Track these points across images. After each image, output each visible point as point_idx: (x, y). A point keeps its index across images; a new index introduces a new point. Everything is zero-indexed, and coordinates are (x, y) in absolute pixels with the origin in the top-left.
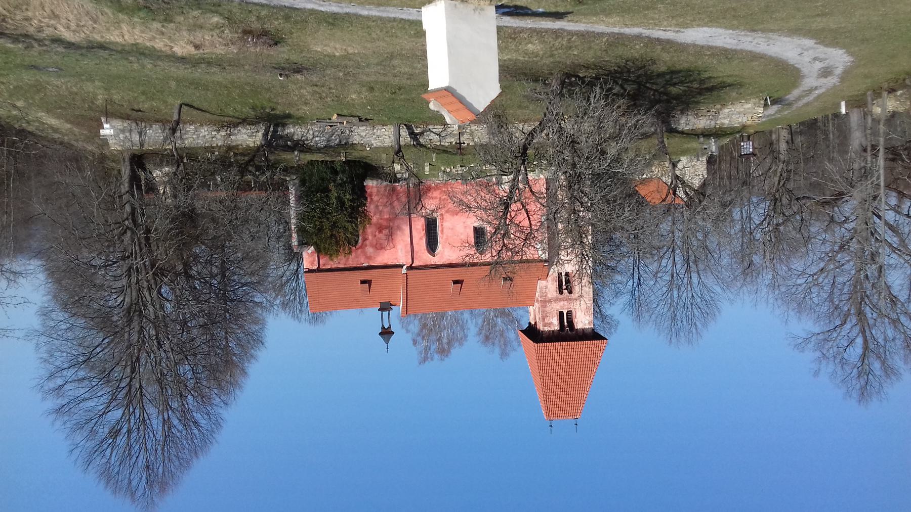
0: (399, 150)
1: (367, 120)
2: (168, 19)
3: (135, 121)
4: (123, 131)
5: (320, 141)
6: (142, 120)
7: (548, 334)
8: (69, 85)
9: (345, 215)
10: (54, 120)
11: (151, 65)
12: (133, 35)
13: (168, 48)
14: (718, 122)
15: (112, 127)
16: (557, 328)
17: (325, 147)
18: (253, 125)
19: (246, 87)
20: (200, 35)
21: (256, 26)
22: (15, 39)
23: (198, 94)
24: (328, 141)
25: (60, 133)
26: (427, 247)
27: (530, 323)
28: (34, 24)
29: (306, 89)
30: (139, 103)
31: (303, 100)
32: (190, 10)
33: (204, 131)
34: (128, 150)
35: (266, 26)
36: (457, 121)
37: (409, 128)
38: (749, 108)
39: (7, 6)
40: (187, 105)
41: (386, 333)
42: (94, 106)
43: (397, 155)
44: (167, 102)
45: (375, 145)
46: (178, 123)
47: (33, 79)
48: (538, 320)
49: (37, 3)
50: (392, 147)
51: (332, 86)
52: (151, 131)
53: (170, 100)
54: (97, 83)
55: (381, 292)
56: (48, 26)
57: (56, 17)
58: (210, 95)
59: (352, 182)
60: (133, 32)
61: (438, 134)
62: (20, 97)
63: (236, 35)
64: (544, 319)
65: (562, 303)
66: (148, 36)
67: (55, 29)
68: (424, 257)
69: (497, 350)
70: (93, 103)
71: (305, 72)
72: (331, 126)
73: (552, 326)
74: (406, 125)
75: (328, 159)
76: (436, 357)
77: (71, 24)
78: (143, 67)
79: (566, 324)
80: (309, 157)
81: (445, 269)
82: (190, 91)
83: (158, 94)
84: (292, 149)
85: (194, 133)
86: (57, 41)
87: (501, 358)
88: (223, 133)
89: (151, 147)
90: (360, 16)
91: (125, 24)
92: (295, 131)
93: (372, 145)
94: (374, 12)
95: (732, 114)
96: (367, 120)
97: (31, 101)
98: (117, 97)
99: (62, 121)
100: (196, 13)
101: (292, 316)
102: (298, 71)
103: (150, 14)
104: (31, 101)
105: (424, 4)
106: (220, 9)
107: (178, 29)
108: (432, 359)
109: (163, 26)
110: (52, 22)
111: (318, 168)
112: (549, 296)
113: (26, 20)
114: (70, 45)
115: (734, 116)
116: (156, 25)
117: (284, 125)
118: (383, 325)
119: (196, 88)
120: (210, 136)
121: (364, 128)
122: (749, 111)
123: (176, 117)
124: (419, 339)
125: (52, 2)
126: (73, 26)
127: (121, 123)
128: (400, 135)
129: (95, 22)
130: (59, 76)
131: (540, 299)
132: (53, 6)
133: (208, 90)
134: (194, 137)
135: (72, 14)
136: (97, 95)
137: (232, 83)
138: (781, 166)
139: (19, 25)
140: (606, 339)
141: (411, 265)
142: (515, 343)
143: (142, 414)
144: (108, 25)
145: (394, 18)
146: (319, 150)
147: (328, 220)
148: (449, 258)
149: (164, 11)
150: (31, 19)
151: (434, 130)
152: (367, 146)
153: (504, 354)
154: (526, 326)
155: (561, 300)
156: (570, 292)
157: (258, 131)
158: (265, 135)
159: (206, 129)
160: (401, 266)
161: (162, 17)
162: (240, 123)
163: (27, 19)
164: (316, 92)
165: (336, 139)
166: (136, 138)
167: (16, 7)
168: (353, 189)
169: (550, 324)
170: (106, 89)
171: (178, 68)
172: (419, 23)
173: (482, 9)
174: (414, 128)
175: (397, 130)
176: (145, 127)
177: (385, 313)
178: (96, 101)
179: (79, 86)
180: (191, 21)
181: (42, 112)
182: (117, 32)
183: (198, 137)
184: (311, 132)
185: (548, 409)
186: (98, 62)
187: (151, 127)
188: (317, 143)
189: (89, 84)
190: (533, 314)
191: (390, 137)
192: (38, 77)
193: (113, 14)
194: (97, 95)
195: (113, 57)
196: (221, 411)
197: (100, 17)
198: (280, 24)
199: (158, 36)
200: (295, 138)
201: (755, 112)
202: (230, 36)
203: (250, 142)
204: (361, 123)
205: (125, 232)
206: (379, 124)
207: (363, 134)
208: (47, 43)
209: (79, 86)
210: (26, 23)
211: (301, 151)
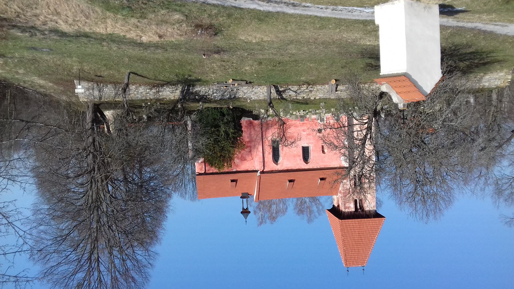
0: (271, 103)
1: (250, 82)
2: (143, 16)
3: (97, 82)
4: (88, 89)
5: (217, 96)
6: (101, 82)
7: (347, 213)
8: (55, 60)
9: (229, 142)
10: (42, 81)
11: (116, 48)
12: (114, 27)
13: (138, 37)
14: (481, 85)
15: (83, 87)
16: (353, 210)
17: (220, 99)
18: (174, 85)
19: (176, 62)
20: (165, 28)
21: (206, 21)
22: (23, 30)
23: (142, 66)
24: (222, 96)
25: (45, 88)
26: (273, 159)
27: (334, 206)
28: (41, 19)
29: (216, 63)
30: (101, 71)
31: (213, 70)
32: (161, 10)
33: (141, 89)
34: (91, 101)
35: (213, 22)
36: (402, 100)
37: (276, 87)
38: (502, 76)
39: (21, 5)
40: (132, 73)
41: (245, 212)
42: (71, 74)
43: (269, 105)
44: (120, 71)
45: (253, 98)
46: (127, 85)
47: (31, 56)
48: (340, 205)
49: (44, 3)
50: (264, 100)
51: (235, 61)
52: (107, 89)
53: (123, 70)
54: (74, 59)
55: (243, 186)
56: (51, 21)
57: (58, 14)
58: (150, 67)
59: (234, 121)
60: (115, 26)
61: (295, 92)
62: (22, 67)
63: (190, 28)
64: (345, 205)
66: (126, 28)
67: (57, 23)
68: (271, 166)
69: (306, 218)
70: (70, 71)
71: (222, 53)
72: (226, 87)
73: (350, 209)
74: (274, 86)
75: (219, 106)
76: (268, 221)
77: (69, 19)
78: (110, 49)
79: (358, 207)
80: (207, 105)
81: (284, 173)
82: (137, 65)
83: (115, 66)
84: (198, 101)
85: (135, 90)
86: (55, 31)
87: (308, 223)
88: (154, 91)
89: (107, 99)
90: (287, 14)
91: (110, 20)
92: (200, 89)
93: (251, 98)
94: (327, 12)
95: (491, 80)
96: (250, 82)
97: (28, 70)
98: (86, 68)
99: (47, 81)
100: (163, 12)
101: (180, 196)
102: (218, 52)
103: (130, 12)
104: (28, 70)
105: (378, 3)
106: (183, 9)
107: (150, 24)
108: (265, 222)
109: (139, 21)
110: (55, 18)
111: (212, 112)
113: (35, 16)
114: (63, 34)
115: (492, 81)
116: (134, 20)
117: (194, 86)
118: (243, 207)
119: (141, 63)
120: (145, 92)
121: (247, 87)
122: (502, 77)
123: (126, 81)
124: (258, 211)
125: (56, 3)
126: (70, 21)
127: (87, 84)
128: (271, 92)
129: (87, 18)
130: (49, 54)
131: (342, 191)
132: (56, 6)
133: (149, 63)
134: (135, 93)
135: (71, 12)
136: (73, 66)
137: (168, 59)
138: (493, 109)
139: (29, 20)
140: (385, 217)
141: (263, 170)
142: (317, 214)
143: (99, 277)
144: (96, 20)
145: (311, 15)
146: (216, 101)
147: (218, 146)
148: (286, 166)
149: (141, 10)
150: (39, 15)
151: (292, 89)
152: (248, 99)
153: (310, 220)
154: (330, 207)
157: (177, 89)
158: (182, 92)
159: (143, 88)
160: (257, 171)
161: (139, 15)
162: (165, 84)
163: (36, 16)
164: (222, 65)
165: (227, 95)
166: (96, 93)
167: (28, 6)
168: (235, 126)
169: (349, 208)
170: (79, 62)
171: (134, 50)
172: (372, 22)
173: (430, 8)
174: (280, 88)
175: (269, 89)
176: (103, 86)
177: (245, 200)
178: (73, 70)
179: (62, 60)
180: (159, 17)
181: (36, 76)
182: (103, 26)
183: (138, 93)
184: (211, 90)
185: (346, 260)
186: (79, 45)
187: (107, 86)
188: (215, 97)
189: (68, 59)
190: (337, 200)
191: (263, 93)
192: (35, 55)
193: (102, 12)
194: (73, 66)
195: (92, 42)
196: (149, 270)
197: (92, 14)
198: (223, 20)
199: (134, 29)
200: (201, 94)
201: (506, 78)
202: (186, 28)
203: (172, 97)
204: (247, 85)
205: (89, 154)
206: (257, 85)
207: (245, 91)
208: (46, 33)
209: (62, 60)
210: (34, 18)
211: (204, 102)
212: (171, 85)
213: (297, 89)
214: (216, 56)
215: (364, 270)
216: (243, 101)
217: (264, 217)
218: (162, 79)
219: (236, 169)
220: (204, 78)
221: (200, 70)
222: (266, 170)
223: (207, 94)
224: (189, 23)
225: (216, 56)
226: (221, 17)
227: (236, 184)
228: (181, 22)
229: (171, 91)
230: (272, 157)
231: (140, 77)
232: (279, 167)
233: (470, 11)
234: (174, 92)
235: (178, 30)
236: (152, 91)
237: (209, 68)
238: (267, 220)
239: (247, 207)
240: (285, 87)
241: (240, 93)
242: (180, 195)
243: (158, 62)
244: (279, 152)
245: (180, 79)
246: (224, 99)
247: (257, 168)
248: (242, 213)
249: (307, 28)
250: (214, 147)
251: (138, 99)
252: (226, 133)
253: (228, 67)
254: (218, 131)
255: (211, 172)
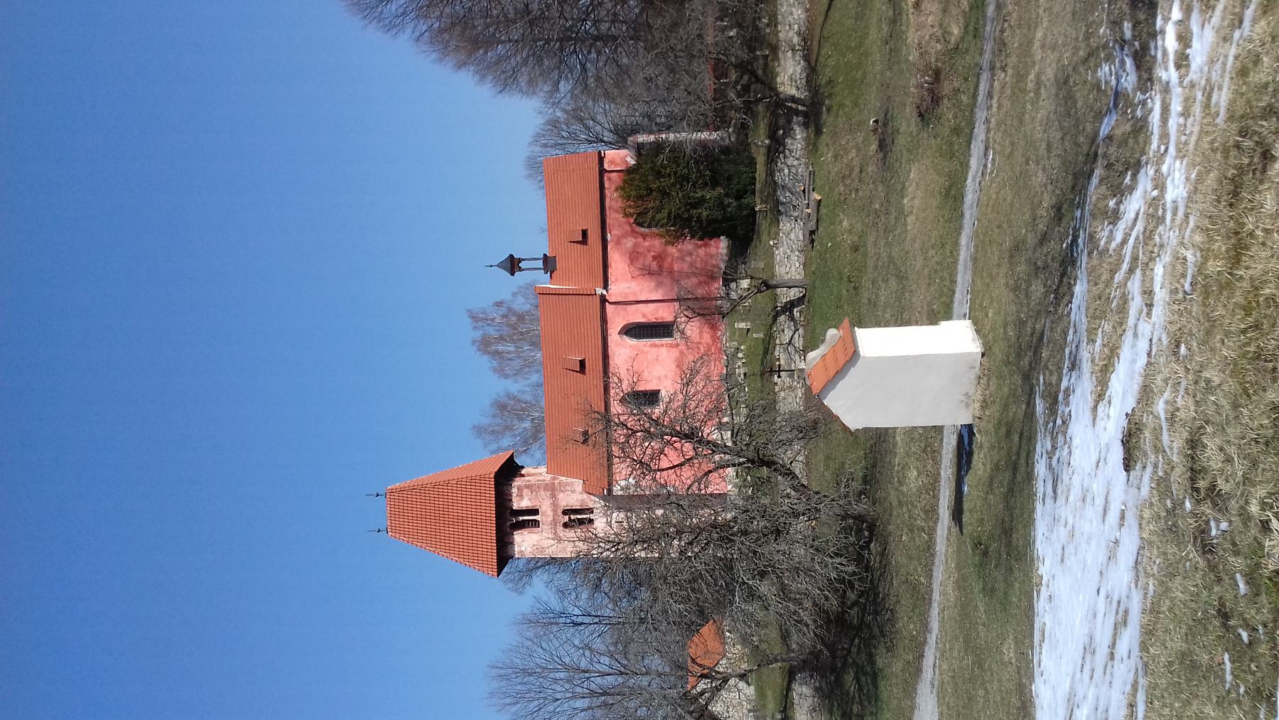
0: (769, 287)
1: (812, 241)
5: (783, 176)
9: (679, 209)
16: (515, 506)
17: (775, 183)
18: (807, 82)
19: (860, 72)
20: (933, 9)
21: (946, 88)
23: (850, 6)
24: (783, 187)
27: (523, 467)
31: (842, 153)
35: (946, 101)
36: (811, 366)
37: (800, 301)
41: (512, 265)
48: (527, 478)
50: (773, 276)
51: (860, 193)
59: (725, 219)
61: (790, 341)
63: (933, 60)
64: (528, 487)
65: (550, 513)
68: (618, 320)
69: (485, 421)
71: (881, 155)
72: (804, 191)
74: (804, 296)
75: (758, 186)
76: (478, 334)
79: (521, 518)
80: (761, 160)
84: (772, 136)
87: (474, 427)
90: (959, 234)
92: (797, 140)
93: (777, 248)
96: (812, 241)
102: (882, 146)
105: (975, 323)
108: (475, 328)
112: (561, 496)
117: (806, 125)
118: (523, 260)
124: (503, 310)
128: (790, 288)
140: (498, 576)
142: (494, 446)
146: (770, 173)
148: (617, 354)
151: (796, 336)
152: (776, 242)
153: (480, 430)
154: (518, 461)
155: (555, 511)
156: (565, 525)
157: (798, 89)
158: (793, 99)
159: (801, 16)
160: (606, 287)
162: (809, 63)
164: (852, 171)
165: (785, 197)
168: (716, 220)
169: (521, 496)
172: (948, 316)
173: (967, 405)
174: (799, 308)
177: (540, 264)
184: (796, 163)
185: (402, 490)
188: (781, 170)
190: (535, 472)
191: (787, 273)
196: (408, 31)
200: (788, 141)
204: (807, 234)
207: (792, 236)
211: (769, 148)
212: (808, 76)
213: (797, 345)
214: (874, 146)
215: (379, 531)
216: (772, 232)
217: (488, 325)
218: (823, 52)
219: (612, 240)
220: (825, 138)
221: (841, 126)
222: (609, 308)
223: (787, 152)
224: (943, 55)
225: (874, 146)
226: (955, 114)
227: (577, 242)
228: (945, 40)
229: (794, 76)
230: (638, 323)
231: (827, 5)
232: (614, 336)
233: (962, 534)
234: (792, 82)
235: (931, 36)
236: (795, 35)
237: (847, 143)
238: (481, 332)
239: (523, 270)
240: (802, 319)
241: (789, 225)
242: (540, 132)
243: (860, 37)
244: (648, 337)
245: (822, 91)
246: (775, 191)
247: (612, 287)
248: (511, 256)
249: (932, 289)
250: (669, 175)
251: (779, 7)
252: (702, 201)
253: (848, 182)
254: (706, 184)
255: (606, 185)
